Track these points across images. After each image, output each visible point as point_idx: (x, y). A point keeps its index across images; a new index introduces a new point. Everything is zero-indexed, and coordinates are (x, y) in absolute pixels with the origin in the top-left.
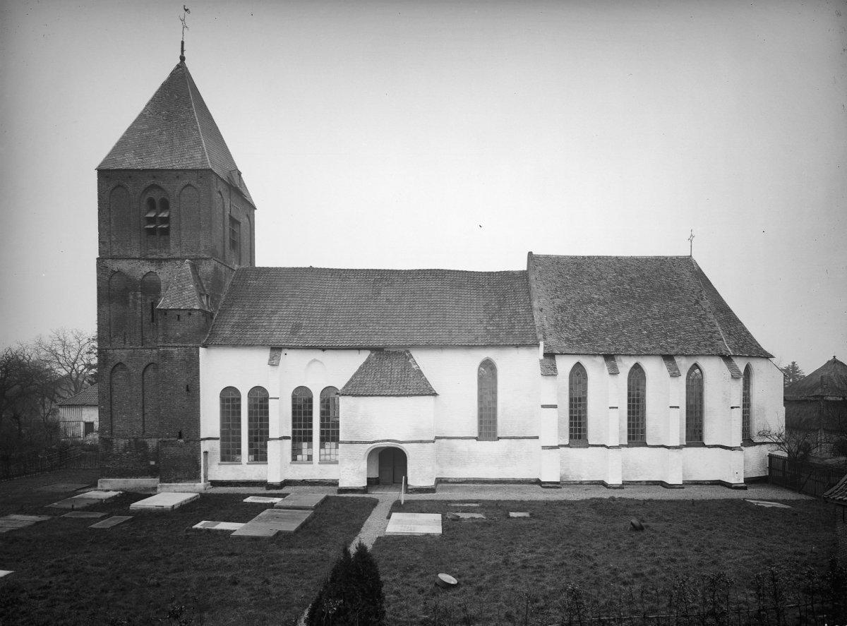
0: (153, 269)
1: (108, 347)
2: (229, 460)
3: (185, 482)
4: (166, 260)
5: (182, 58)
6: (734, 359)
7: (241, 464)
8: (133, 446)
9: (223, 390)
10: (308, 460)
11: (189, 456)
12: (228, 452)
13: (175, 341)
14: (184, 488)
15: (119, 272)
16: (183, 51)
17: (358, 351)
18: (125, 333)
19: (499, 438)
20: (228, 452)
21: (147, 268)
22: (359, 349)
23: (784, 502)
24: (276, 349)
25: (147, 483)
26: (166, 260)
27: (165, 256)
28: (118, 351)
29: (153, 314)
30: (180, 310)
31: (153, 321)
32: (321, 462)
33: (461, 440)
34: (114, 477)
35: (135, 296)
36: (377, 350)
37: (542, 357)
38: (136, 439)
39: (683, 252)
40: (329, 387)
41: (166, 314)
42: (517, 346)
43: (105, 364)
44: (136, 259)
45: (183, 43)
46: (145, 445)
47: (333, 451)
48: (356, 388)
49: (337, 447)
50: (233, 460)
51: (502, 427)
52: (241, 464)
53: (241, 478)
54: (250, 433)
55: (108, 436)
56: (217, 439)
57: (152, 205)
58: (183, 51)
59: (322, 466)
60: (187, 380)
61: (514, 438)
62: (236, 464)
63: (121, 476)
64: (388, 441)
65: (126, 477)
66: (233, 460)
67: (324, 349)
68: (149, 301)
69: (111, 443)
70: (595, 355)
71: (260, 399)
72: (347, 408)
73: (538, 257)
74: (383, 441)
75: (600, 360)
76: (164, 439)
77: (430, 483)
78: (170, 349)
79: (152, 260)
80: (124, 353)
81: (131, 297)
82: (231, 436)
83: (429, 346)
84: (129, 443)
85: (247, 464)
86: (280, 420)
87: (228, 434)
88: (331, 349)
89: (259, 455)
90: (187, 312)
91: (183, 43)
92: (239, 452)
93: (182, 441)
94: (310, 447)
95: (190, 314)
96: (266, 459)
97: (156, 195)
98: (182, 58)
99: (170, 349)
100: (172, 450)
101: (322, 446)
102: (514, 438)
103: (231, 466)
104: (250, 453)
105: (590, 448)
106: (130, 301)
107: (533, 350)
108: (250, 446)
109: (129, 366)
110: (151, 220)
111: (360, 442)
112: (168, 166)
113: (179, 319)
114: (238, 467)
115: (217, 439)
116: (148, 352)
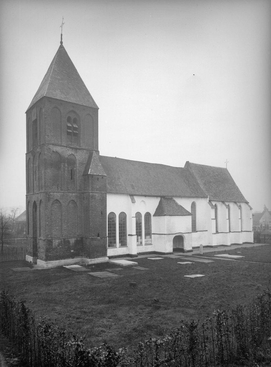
0: (73, 153)
1: (50, 191)
2: (111, 246)
3: (101, 257)
4: (79, 149)
5: (61, 43)
6: (225, 202)
7: (117, 248)
8: (63, 243)
9: (110, 213)
10: (141, 244)
11: (102, 245)
12: (111, 243)
13: (96, 190)
14: (152, 256)
15: (57, 152)
16: (62, 39)
17: (156, 198)
18: (58, 184)
19: (197, 232)
20: (111, 243)
21: (70, 152)
22: (157, 196)
23: (179, 255)
24: (132, 195)
25: (69, 261)
26: (79, 149)
27: (78, 147)
28: (56, 193)
29: (72, 175)
30: (99, 175)
31: (72, 179)
32: (146, 244)
33: (205, 232)
34: (53, 260)
35: (64, 165)
36: (162, 197)
37: (208, 202)
38: (64, 239)
39: (223, 166)
40: (114, 213)
41: (92, 177)
42: (202, 197)
43: (49, 200)
44: (64, 146)
45: (62, 35)
46: (69, 242)
47: (149, 239)
48: (160, 212)
49: (151, 238)
50: (113, 246)
51: (198, 228)
52: (117, 248)
53: (116, 254)
54: (120, 233)
55: (50, 239)
56: (153, 234)
57: (69, 120)
58: (62, 39)
59: (145, 246)
60: (102, 208)
61: (201, 231)
62: (114, 248)
63: (57, 259)
64: (180, 233)
65: (59, 260)
66: (113, 246)
67: (145, 196)
68: (70, 169)
69: (52, 242)
70: (220, 201)
71: (123, 216)
72: (154, 221)
73: (190, 163)
74: (178, 233)
75: (221, 203)
76: (92, 238)
77: (191, 249)
78: (95, 194)
79: (72, 148)
80: (59, 194)
81: (62, 166)
82: (112, 235)
83: (180, 197)
84: (61, 242)
85: (119, 247)
86: (131, 228)
87: (111, 234)
88: (140, 196)
89: (123, 243)
90: (101, 177)
91: (62, 35)
92: (115, 243)
93: (99, 238)
94: (141, 238)
95: (102, 178)
96: (126, 245)
97: (73, 116)
98: (61, 43)
99: (95, 194)
100: (95, 242)
101: (145, 238)
102: (201, 231)
103: (112, 249)
104: (120, 243)
105: (219, 234)
106: (62, 168)
107: (205, 199)
108: (120, 239)
109: (61, 201)
110: (69, 128)
111: (172, 234)
112: (80, 103)
113: (98, 180)
114: (115, 249)
115: (153, 234)
116: (71, 194)
